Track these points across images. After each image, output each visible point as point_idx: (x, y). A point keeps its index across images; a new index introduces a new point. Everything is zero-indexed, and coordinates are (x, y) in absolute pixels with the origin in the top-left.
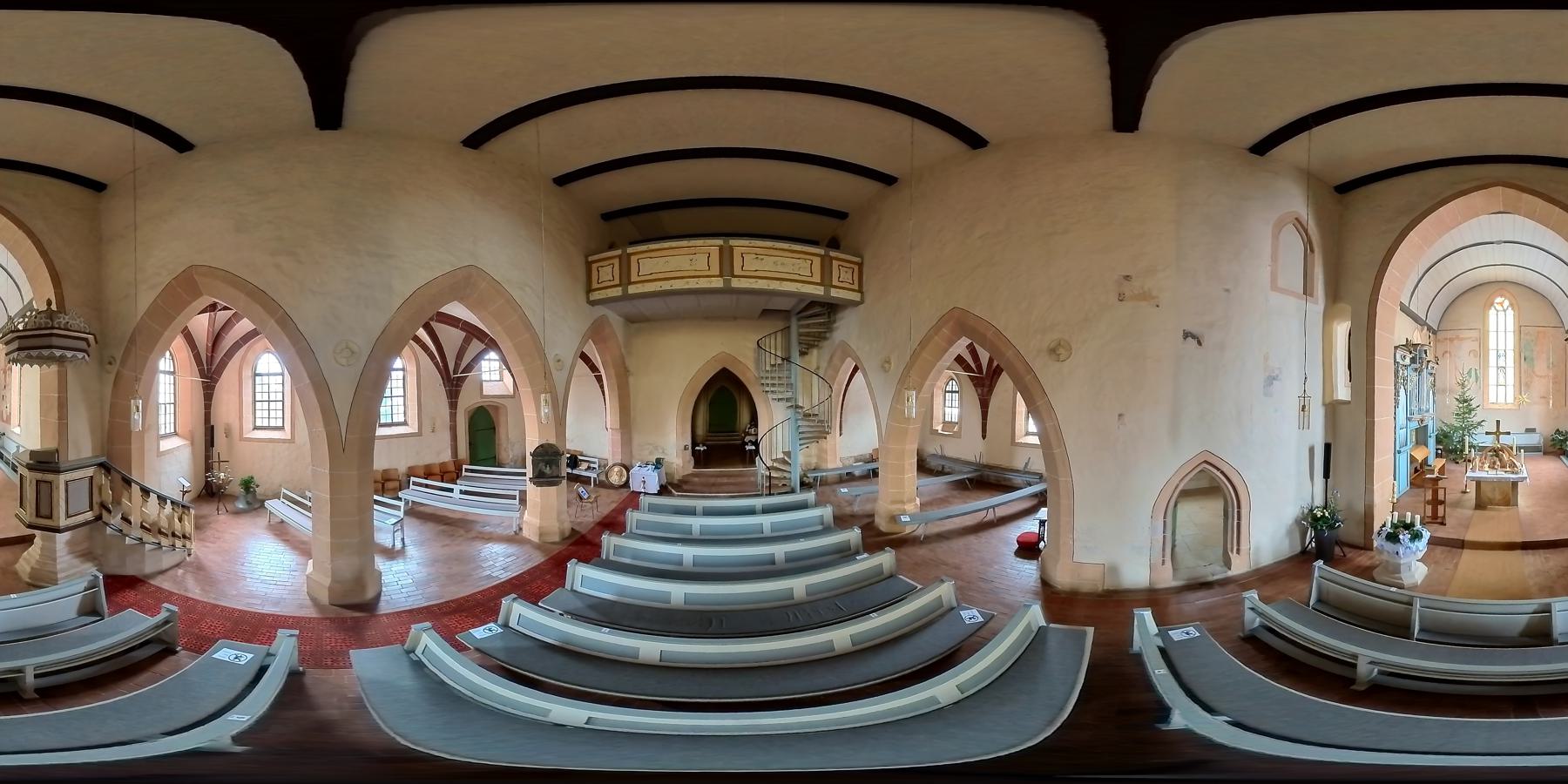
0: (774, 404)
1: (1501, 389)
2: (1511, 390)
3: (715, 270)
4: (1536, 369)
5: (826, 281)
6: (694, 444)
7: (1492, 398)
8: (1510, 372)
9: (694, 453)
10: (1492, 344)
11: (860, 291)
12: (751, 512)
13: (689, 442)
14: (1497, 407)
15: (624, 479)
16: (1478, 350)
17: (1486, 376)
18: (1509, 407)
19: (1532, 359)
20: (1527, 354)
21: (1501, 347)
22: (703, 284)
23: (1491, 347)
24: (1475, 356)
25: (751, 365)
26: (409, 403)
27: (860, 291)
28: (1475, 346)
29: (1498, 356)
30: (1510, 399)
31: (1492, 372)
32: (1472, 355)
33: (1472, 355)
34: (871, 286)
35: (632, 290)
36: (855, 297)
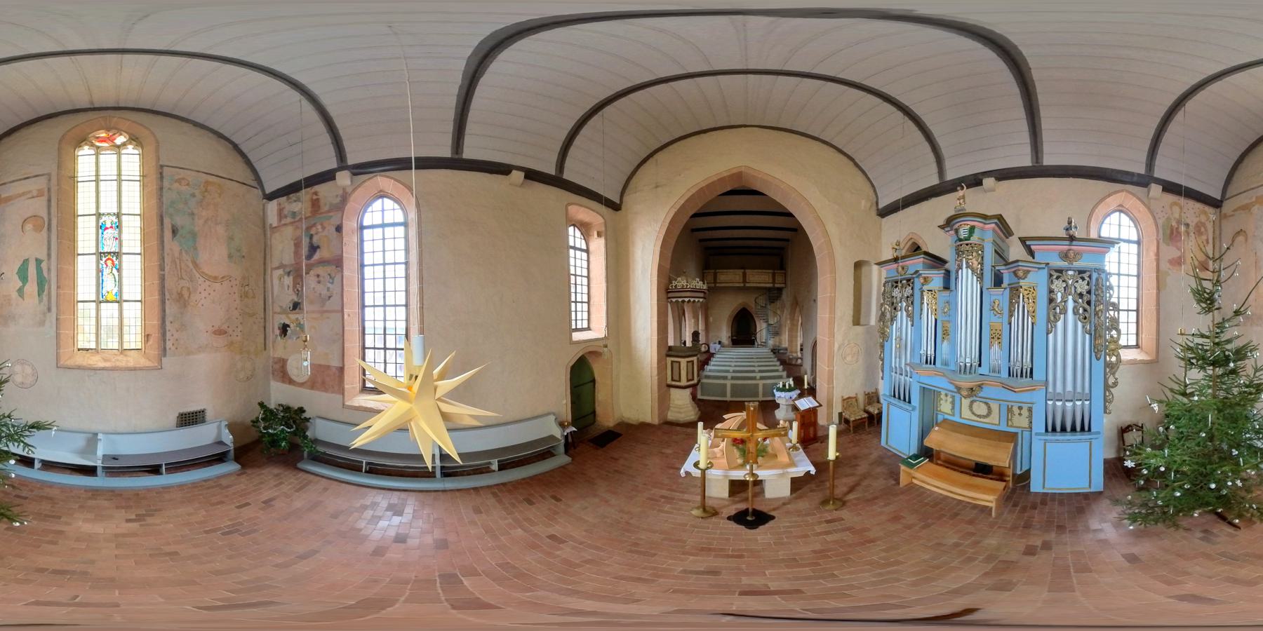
0: (762, 321)
1: (109, 310)
2: (133, 313)
3: (741, 281)
4: (203, 257)
5: (774, 282)
6: (732, 336)
7: (85, 339)
8: (133, 268)
9: (732, 340)
10: (85, 200)
11: (785, 283)
12: (754, 366)
13: (730, 335)
14: (96, 361)
15: (707, 349)
16: (44, 214)
17: (68, 278)
18: (131, 360)
19: (194, 235)
20: (179, 221)
21: (109, 206)
22: (738, 285)
23: (571, 255)
24: (38, 229)
25: (753, 306)
26: (1144, 322)
27: (785, 283)
28: (39, 206)
29: (100, 228)
30: (134, 339)
31: (85, 268)
32: (29, 227)
33: (29, 227)
34: (789, 283)
35: (748, 285)
36: (783, 285)
